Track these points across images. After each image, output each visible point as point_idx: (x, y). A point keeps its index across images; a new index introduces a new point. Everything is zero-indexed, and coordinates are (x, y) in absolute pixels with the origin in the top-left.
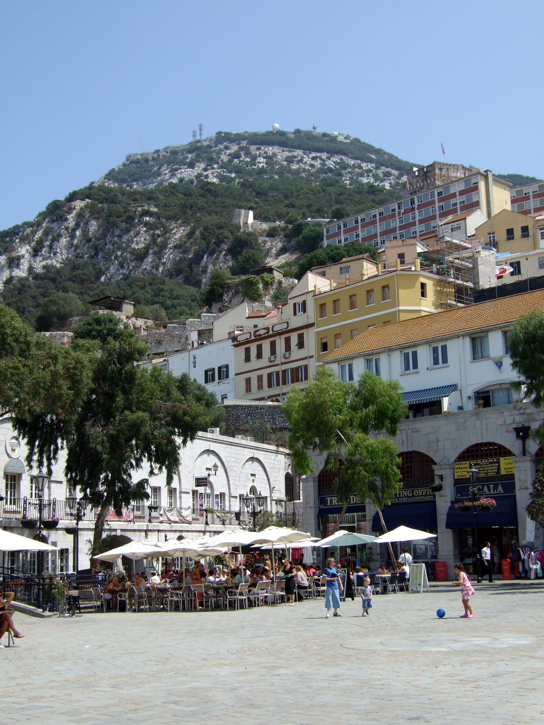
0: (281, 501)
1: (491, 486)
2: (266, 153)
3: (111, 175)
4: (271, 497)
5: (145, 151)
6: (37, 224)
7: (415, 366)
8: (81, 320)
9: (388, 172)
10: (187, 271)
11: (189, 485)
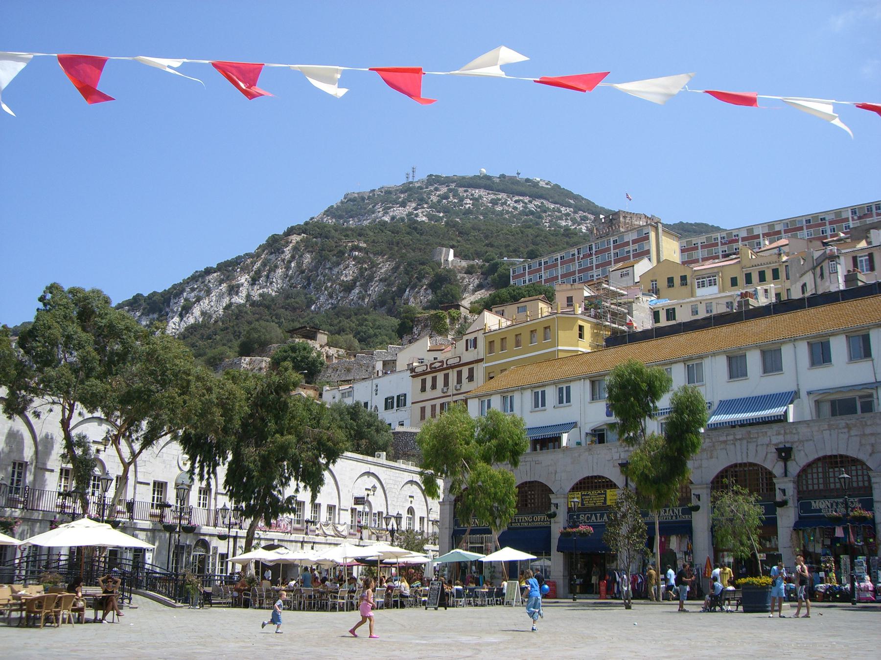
0: (437, 521)
1: (598, 515)
2: (472, 195)
3: (329, 212)
4: (428, 517)
5: (362, 190)
6: (257, 255)
7: (543, 404)
8: (278, 348)
9: (585, 216)
10: (388, 302)
11: (348, 503)
